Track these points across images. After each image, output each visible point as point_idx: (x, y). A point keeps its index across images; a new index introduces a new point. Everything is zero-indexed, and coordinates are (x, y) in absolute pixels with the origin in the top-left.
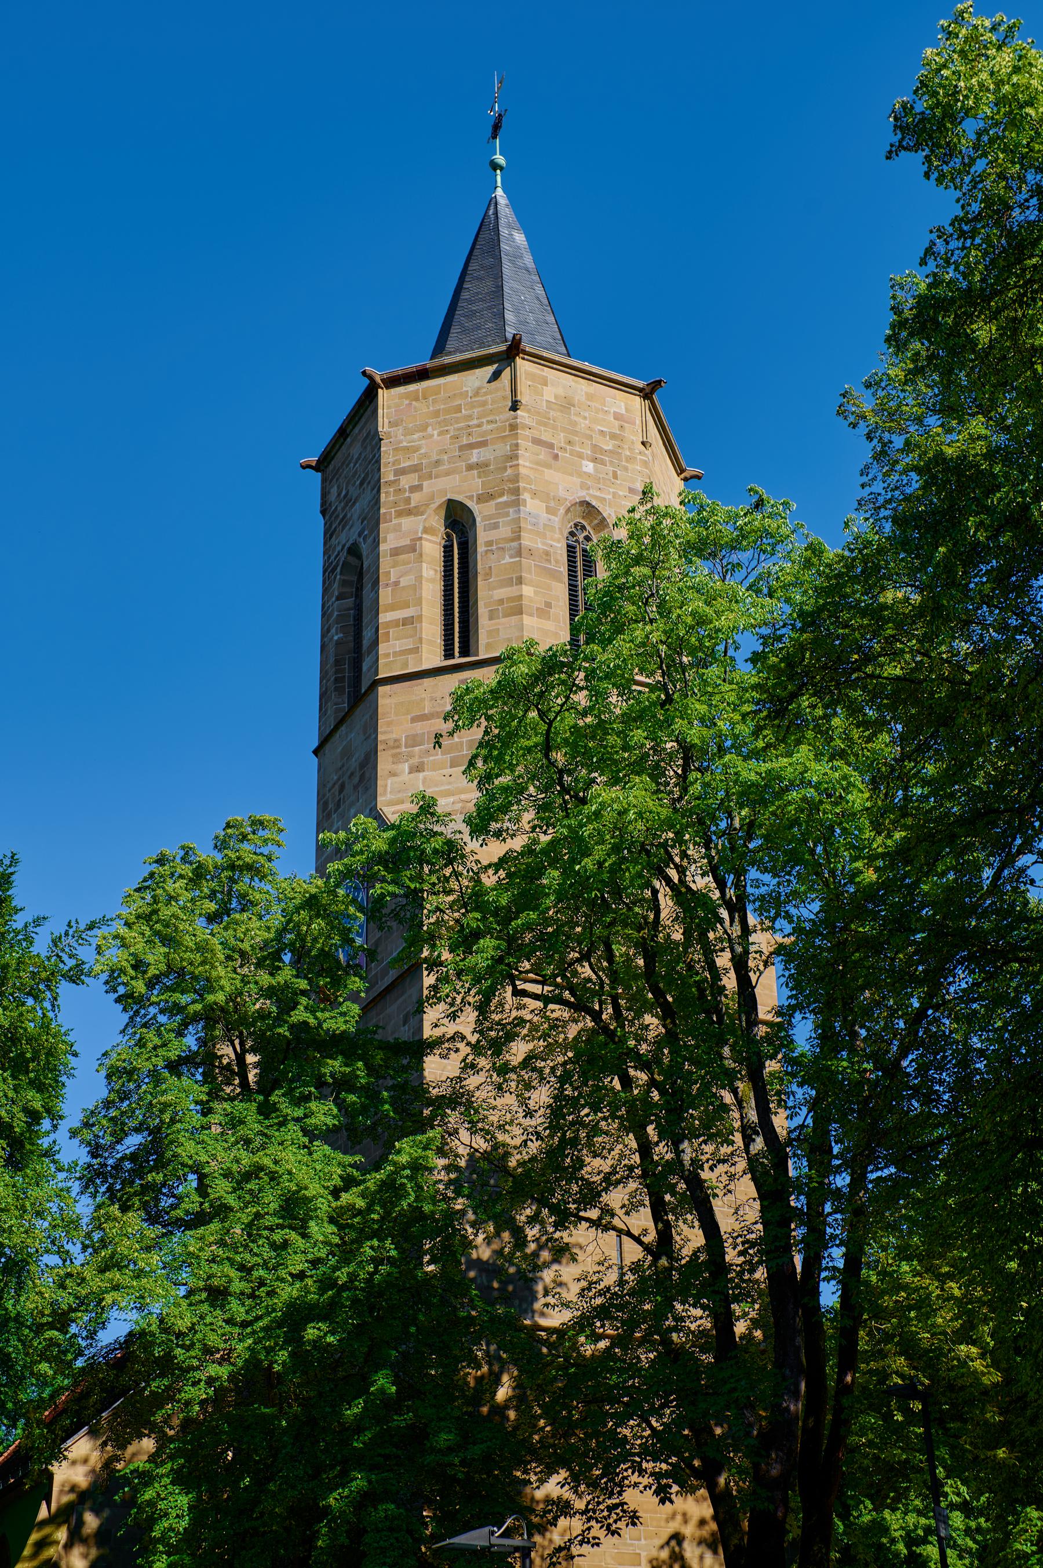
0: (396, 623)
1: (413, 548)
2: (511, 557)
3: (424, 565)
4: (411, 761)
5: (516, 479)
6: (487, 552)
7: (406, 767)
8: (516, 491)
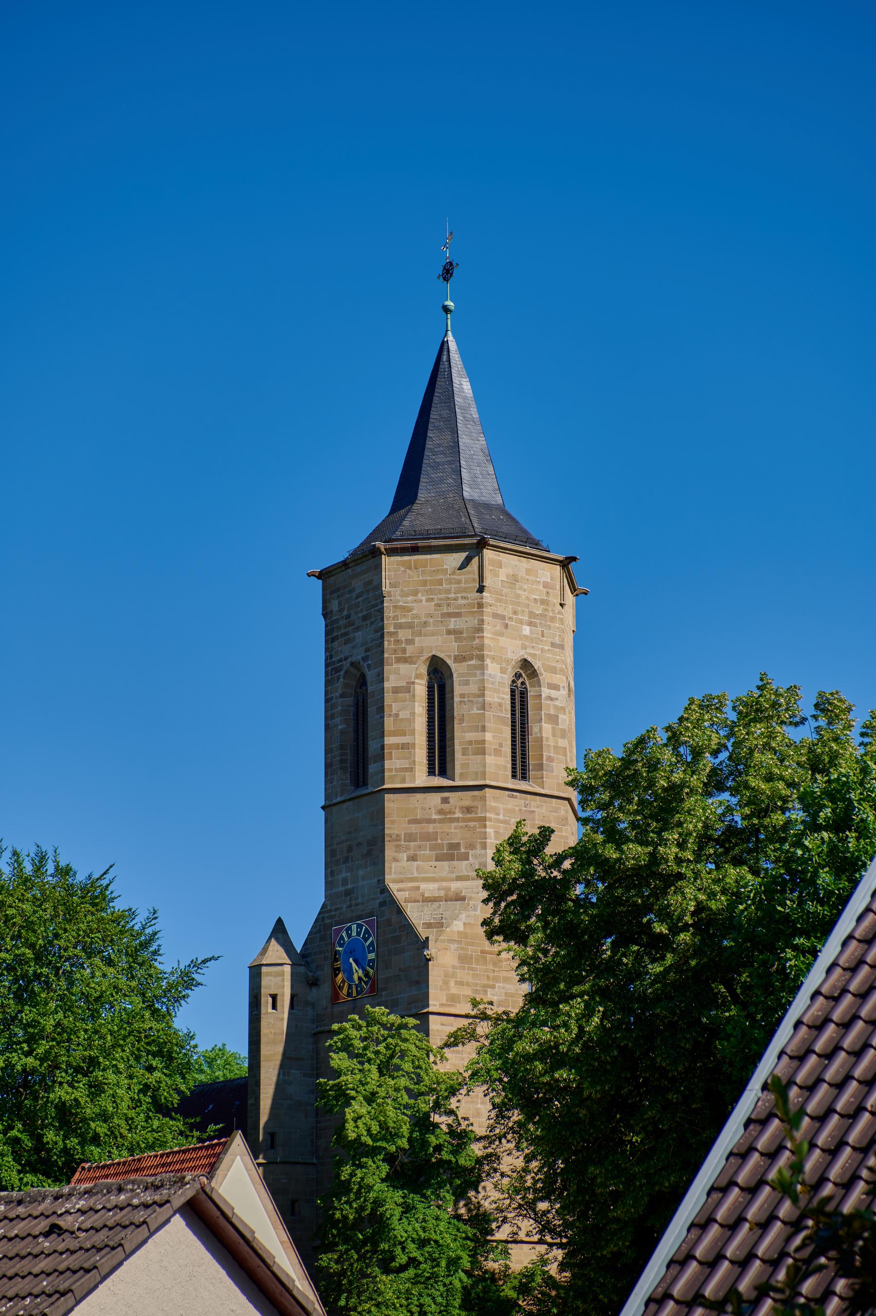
0: (397, 746)
1: (408, 689)
2: (478, 709)
3: (416, 704)
4: (408, 852)
5: (481, 648)
6: (461, 702)
7: (404, 856)
8: (482, 658)
